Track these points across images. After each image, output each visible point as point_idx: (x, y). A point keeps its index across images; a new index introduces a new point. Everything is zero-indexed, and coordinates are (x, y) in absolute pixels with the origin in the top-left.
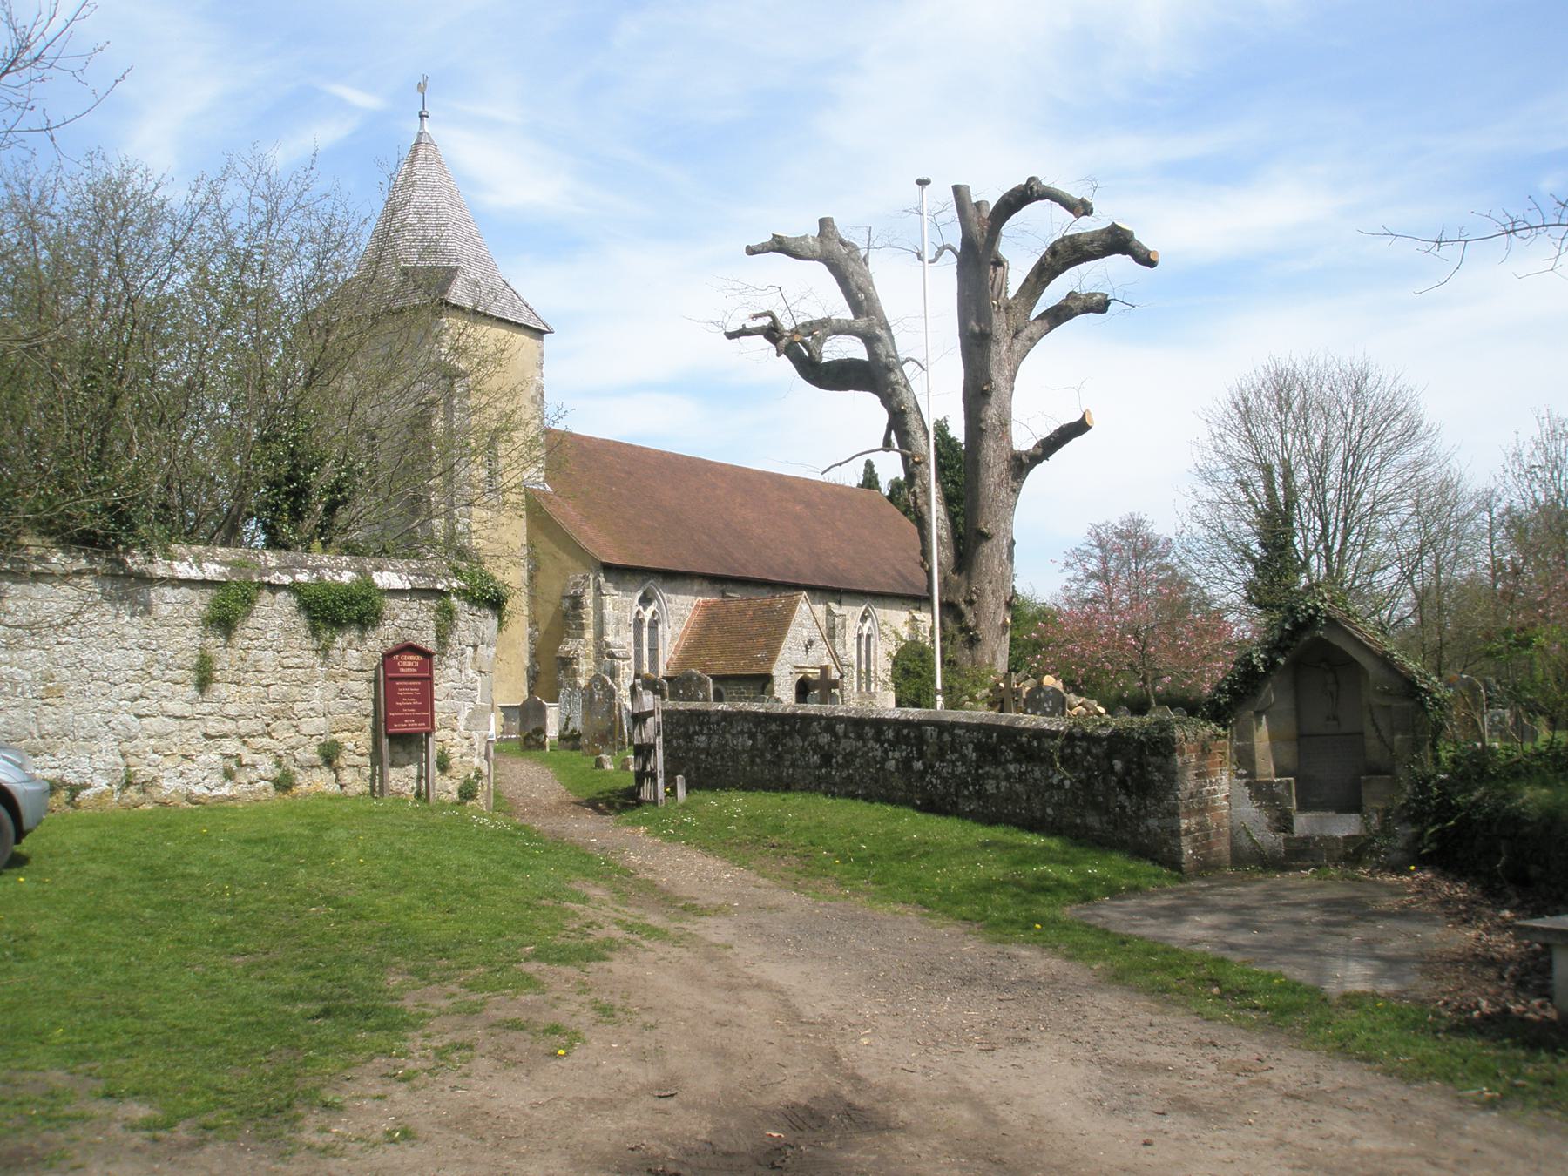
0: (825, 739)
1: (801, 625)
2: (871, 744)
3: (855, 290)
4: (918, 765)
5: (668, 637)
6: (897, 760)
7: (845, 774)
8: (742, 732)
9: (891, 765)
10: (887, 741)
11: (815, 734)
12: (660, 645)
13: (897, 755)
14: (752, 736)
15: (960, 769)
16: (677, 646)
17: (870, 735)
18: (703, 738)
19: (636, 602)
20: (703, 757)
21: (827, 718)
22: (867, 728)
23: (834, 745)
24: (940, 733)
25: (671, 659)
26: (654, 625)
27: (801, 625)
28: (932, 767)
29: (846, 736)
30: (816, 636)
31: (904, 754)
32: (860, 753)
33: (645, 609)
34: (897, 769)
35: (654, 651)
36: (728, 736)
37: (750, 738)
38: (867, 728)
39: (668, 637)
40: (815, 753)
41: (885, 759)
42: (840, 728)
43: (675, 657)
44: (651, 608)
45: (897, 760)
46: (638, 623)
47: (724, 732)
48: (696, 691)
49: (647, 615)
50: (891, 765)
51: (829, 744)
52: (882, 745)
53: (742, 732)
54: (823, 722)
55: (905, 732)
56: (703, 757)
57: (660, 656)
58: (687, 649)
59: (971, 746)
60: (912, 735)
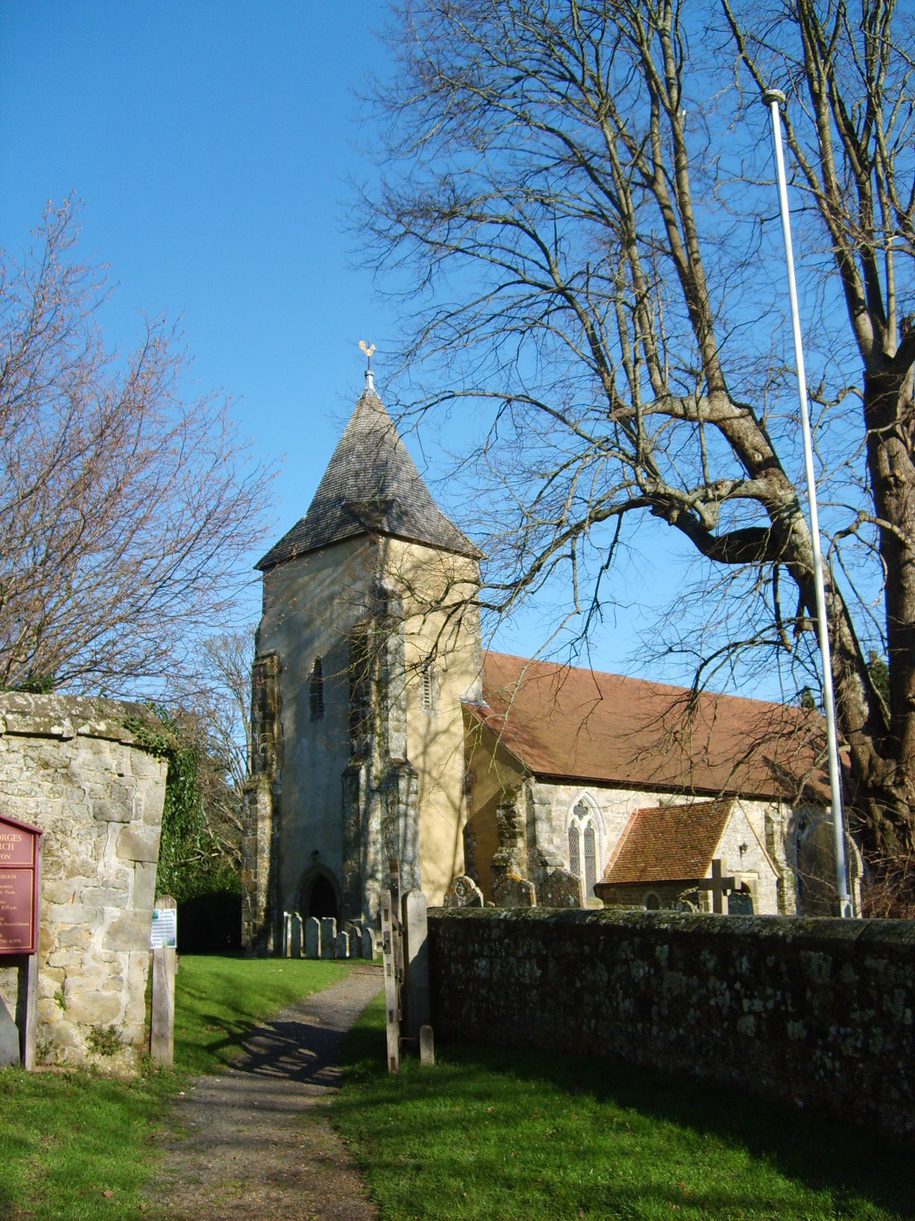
0: (641, 970)
1: (735, 830)
2: (713, 982)
3: (751, 451)
4: (794, 1028)
5: (605, 845)
6: (757, 1015)
7: (673, 1036)
8: (528, 956)
9: (748, 1024)
10: (738, 977)
11: (626, 962)
12: (597, 853)
13: (758, 1005)
14: (542, 963)
15: (880, 1043)
16: (614, 854)
17: (711, 965)
18: (483, 963)
19: (572, 810)
20: (483, 991)
21: (642, 933)
22: (705, 954)
23: (654, 981)
24: (836, 968)
25: (608, 866)
26: (589, 834)
27: (735, 830)
28: (824, 1035)
29: (671, 966)
30: (750, 841)
31: (770, 1005)
32: (694, 999)
33: (581, 817)
34: (759, 1033)
35: (591, 858)
36: (512, 960)
37: (539, 967)
38: (705, 954)
39: (605, 845)
40: (626, 995)
41: (736, 1013)
42: (661, 952)
43: (612, 865)
44: (586, 818)
45: (757, 1015)
46: (573, 833)
47: (507, 955)
48: (565, 895)
49: (582, 825)
50: (748, 1024)
51: (647, 977)
52: (731, 987)
53: (528, 956)
54: (637, 940)
55: (770, 960)
56: (483, 991)
57: (598, 864)
58: (623, 855)
59: (900, 994)
60: (783, 968)
